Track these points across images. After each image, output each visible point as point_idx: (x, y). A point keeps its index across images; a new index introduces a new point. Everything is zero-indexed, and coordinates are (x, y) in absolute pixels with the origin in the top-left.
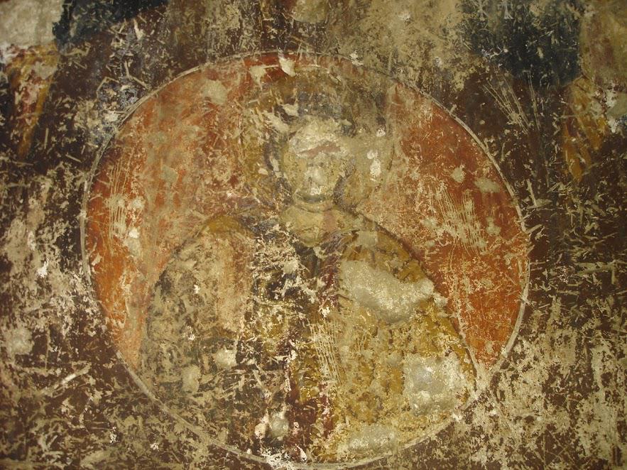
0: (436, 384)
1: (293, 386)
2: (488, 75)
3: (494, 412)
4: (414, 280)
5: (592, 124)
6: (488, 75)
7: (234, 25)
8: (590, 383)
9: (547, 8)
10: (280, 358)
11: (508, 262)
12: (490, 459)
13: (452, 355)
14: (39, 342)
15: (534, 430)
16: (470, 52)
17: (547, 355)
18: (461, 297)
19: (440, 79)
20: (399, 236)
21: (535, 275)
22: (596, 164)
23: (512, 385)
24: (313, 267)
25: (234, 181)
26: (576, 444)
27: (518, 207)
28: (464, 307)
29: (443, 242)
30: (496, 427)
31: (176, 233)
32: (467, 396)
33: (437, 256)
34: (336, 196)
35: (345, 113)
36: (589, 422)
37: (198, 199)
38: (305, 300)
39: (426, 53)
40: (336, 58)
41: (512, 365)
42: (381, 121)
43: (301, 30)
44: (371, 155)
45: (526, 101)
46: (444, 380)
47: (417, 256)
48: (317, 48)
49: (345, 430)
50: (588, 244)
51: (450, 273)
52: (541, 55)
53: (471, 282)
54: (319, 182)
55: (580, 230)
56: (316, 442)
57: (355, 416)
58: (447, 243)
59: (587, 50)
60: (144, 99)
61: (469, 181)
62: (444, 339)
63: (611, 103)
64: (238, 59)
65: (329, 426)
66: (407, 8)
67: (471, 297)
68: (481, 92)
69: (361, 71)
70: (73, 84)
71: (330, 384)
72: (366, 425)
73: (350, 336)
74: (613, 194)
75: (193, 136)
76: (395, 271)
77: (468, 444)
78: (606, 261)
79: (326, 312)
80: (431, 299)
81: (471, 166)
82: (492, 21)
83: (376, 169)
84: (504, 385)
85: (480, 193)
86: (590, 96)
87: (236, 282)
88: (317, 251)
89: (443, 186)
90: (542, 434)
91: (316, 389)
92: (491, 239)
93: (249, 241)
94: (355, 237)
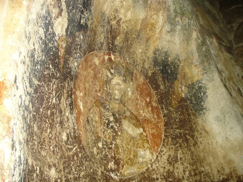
1: (114, 154)
2: (157, 73)
3: (157, 165)
4: (138, 127)
5: (178, 93)
6: (157, 73)
7: (102, 41)
8: (177, 160)
9: (173, 59)
10: (111, 146)
11: (159, 126)
12: (156, 177)
13: (148, 149)
15: (165, 170)
16: (153, 66)
17: (168, 152)
18: (149, 134)
19: (146, 71)
20: (134, 114)
21: (165, 130)
22: (179, 104)
23: (161, 158)
24: (117, 120)
26: (174, 174)
27: (161, 112)
28: (150, 137)
29: (144, 118)
30: (158, 169)
32: (151, 160)
33: (143, 121)
34: (121, 100)
35: (124, 76)
36: (177, 169)
37: (92, 95)
38: (115, 130)
39: (144, 63)
40: (124, 58)
41: (161, 153)
43: (117, 47)
44: (129, 89)
45: (165, 83)
46: (146, 155)
47: (138, 121)
48: (120, 54)
49: (126, 168)
50: (176, 125)
51: (146, 127)
52: (169, 72)
53: (151, 130)
54: (117, 94)
55: (175, 121)
56: (120, 170)
57: (128, 164)
58: (145, 118)
59: (180, 74)
60: (82, 59)
61: (150, 102)
62: (146, 145)
63: (183, 89)
64: (102, 52)
65: (123, 166)
66: (141, 49)
67: (151, 134)
68: (155, 78)
69: (129, 63)
72: (130, 166)
73: (125, 142)
74: (182, 113)
75: (91, 74)
76: (134, 124)
77: (152, 173)
78: (181, 130)
79: (119, 133)
80: (142, 133)
81: (151, 98)
82: (160, 59)
83: (130, 94)
84: (159, 158)
85: (152, 106)
86: (179, 86)
87: (101, 122)
88: (117, 115)
89: (144, 102)
90: (211, 171)
91: (119, 155)
92: (155, 119)
93: (102, 110)
94: (125, 113)
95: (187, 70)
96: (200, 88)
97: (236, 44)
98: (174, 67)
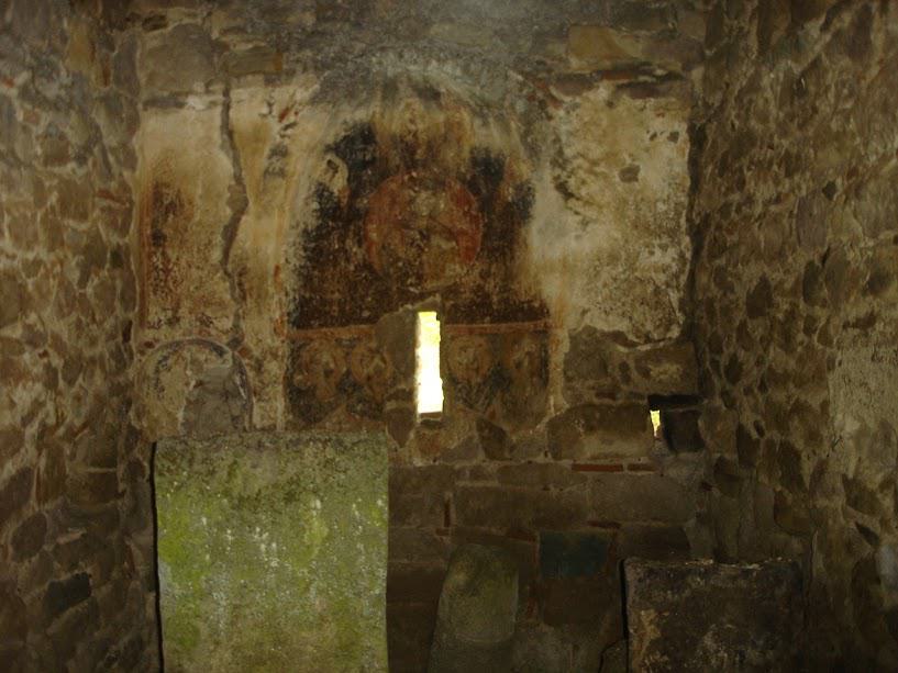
14: (356, 267)
25: (400, 213)
31: (386, 231)
42: (444, 190)
46: (455, 269)
62: (457, 259)
70: (354, 195)
71: (427, 269)
79: (426, 250)
83: (442, 206)
96: (529, 189)
98: (499, 164)
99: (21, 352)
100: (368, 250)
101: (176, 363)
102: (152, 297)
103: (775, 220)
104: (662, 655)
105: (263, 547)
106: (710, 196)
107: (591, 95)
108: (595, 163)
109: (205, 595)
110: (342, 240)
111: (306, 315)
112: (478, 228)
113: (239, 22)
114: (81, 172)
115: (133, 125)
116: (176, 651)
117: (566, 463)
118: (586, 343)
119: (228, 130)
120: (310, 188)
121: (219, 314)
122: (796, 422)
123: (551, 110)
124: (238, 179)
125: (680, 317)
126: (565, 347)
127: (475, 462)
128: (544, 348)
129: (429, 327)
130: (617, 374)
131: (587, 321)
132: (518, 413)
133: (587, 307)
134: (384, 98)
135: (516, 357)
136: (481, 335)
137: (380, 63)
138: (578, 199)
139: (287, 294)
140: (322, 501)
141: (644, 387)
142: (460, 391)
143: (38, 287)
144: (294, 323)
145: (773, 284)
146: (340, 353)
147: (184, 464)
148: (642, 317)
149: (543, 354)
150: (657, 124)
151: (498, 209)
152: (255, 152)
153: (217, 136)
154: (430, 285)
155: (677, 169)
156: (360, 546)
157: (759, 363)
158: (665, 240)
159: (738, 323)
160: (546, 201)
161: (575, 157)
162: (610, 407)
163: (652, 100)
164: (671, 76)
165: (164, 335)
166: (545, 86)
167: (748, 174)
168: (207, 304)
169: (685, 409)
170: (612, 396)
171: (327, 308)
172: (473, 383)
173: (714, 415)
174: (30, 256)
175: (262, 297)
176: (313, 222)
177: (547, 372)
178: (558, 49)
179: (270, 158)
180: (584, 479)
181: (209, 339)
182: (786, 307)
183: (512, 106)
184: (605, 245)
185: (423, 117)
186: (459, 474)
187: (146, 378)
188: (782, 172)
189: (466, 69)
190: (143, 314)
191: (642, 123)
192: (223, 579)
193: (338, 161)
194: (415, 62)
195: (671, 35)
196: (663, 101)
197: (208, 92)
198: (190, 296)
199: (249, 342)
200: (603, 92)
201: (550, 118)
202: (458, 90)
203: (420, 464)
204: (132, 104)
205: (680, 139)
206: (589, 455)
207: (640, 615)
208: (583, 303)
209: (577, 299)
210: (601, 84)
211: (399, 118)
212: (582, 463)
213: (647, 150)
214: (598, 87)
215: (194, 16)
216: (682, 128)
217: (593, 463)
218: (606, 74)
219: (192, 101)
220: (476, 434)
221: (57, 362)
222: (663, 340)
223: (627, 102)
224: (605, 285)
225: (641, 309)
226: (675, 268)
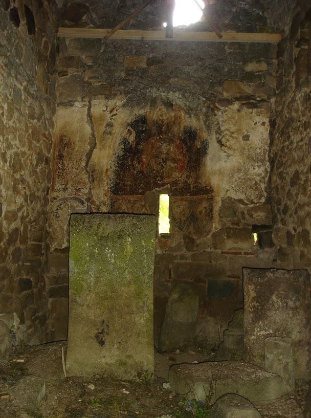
0: (176, 175)
42: (173, 143)
46: (176, 175)
47: (175, 160)
62: (177, 170)
70: (137, 144)
95: (201, 134)
97: (41, 245)
99: (19, 184)
100: (142, 166)
101: (64, 207)
102: (57, 179)
103: (301, 148)
104: (256, 303)
105: (109, 255)
106: (277, 145)
107: (231, 107)
108: (232, 133)
109: (86, 273)
110: (132, 161)
111: (117, 190)
112: (186, 158)
113: (96, 74)
114: (39, 124)
115: (54, 111)
116: (74, 294)
117: (219, 251)
118: (227, 203)
119: (89, 115)
120: (121, 140)
121: (83, 187)
122: (308, 220)
123: (216, 112)
124: (93, 135)
125: (265, 194)
126: (220, 204)
127: (182, 253)
128: (211, 205)
129: (164, 200)
130: (240, 216)
131: (228, 194)
132: (200, 232)
133: (228, 189)
134: (151, 106)
135: (199, 210)
136: (186, 201)
137: (150, 92)
138: (225, 147)
139: (110, 180)
140: (131, 239)
141: (251, 221)
142: (177, 223)
143: (25, 161)
144: (112, 192)
145: (300, 172)
146: (129, 206)
147: (81, 223)
148: (250, 194)
149: (211, 207)
150: (257, 119)
151: (194, 151)
152: (100, 124)
153: (85, 117)
154: (166, 181)
155: (265, 136)
156: (145, 256)
157: (295, 202)
158: (260, 163)
159: (287, 191)
160: (213, 147)
161: (225, 130)
162: (237, 229)
163: (255, 109)
164: (263, 101)
165: (61, 195)
166: (213, 103)
167: (291, 133)
168: (79, 183)
169: (267, 231)
170: (238, 224)
171: (125, 188)
172: (182, 220)
173: (278, 230)
174: (23, 150)
175: (101, 181)
176: (121, 153)
177: (212, 214)
178: (220, 89)
179: (106, 127)
180: (226, 258)
181: (79, 197)
182: (305, 179)
183: (201, 110)
184: (236, 165)
185: (165, 114)
186: (175, 257)
187: (52, 212)
188: (303, 129)
189: (183, 95)
190: (53, 186)
191: (251, 118)
192: (93, 266)
193: (132, 130)
194: (164, 92)
195: (263, 85)
196: (259, 110)
197: (82, 101)
198: (72, 179)
199: (95, 198)
200: (236, 106)
201: (215, 115)
202: (179, 103)
203: (160, 253)
204: (54, 104)
205: (266, 125)
206: (228, 248)
207: (248, 287)
208: (227, 187)
209: (225, 185)
210: (235, 103)
211: (157, 114)
212: (226, 251)
213: (253, 128)
214: (234, 104)
215: (78, 71)
216: (267, 121)
217: (229, 251)
218: (237, 99)
219: (76, 104)
220: (182, 240)
221: (28, 193)
222: (258, 203)
223: (245, 110)
224: (236, 181)
225: (250, 190)
226: (263, 175)
